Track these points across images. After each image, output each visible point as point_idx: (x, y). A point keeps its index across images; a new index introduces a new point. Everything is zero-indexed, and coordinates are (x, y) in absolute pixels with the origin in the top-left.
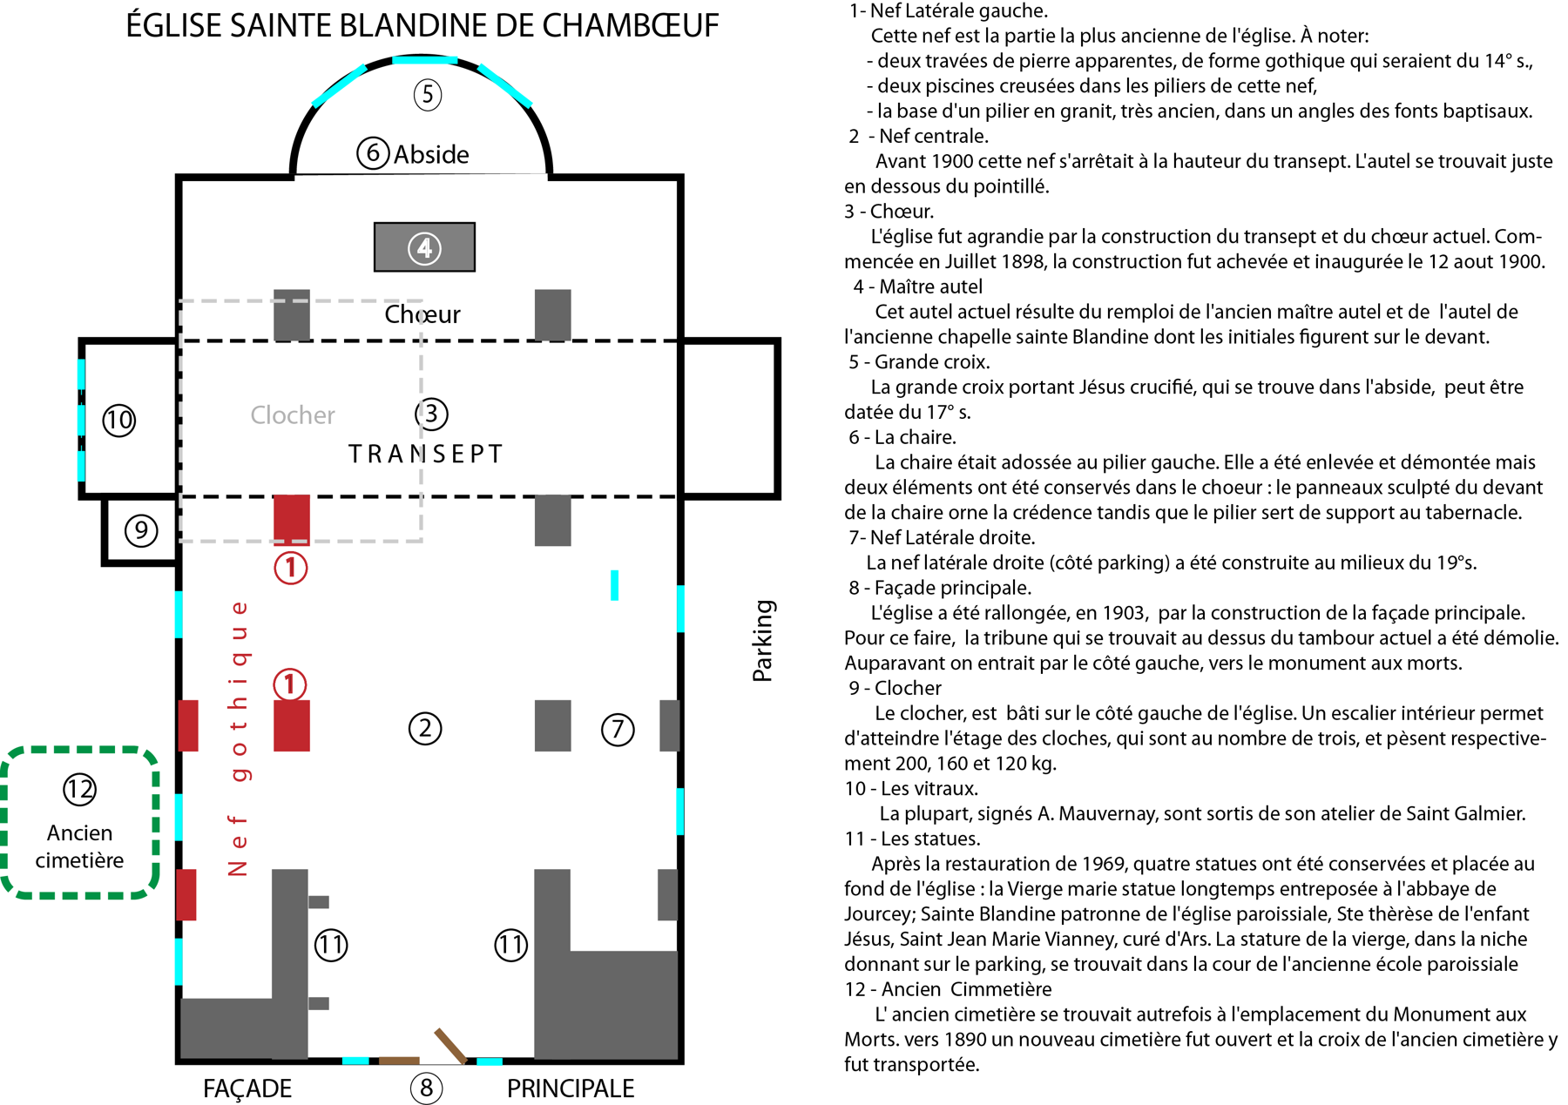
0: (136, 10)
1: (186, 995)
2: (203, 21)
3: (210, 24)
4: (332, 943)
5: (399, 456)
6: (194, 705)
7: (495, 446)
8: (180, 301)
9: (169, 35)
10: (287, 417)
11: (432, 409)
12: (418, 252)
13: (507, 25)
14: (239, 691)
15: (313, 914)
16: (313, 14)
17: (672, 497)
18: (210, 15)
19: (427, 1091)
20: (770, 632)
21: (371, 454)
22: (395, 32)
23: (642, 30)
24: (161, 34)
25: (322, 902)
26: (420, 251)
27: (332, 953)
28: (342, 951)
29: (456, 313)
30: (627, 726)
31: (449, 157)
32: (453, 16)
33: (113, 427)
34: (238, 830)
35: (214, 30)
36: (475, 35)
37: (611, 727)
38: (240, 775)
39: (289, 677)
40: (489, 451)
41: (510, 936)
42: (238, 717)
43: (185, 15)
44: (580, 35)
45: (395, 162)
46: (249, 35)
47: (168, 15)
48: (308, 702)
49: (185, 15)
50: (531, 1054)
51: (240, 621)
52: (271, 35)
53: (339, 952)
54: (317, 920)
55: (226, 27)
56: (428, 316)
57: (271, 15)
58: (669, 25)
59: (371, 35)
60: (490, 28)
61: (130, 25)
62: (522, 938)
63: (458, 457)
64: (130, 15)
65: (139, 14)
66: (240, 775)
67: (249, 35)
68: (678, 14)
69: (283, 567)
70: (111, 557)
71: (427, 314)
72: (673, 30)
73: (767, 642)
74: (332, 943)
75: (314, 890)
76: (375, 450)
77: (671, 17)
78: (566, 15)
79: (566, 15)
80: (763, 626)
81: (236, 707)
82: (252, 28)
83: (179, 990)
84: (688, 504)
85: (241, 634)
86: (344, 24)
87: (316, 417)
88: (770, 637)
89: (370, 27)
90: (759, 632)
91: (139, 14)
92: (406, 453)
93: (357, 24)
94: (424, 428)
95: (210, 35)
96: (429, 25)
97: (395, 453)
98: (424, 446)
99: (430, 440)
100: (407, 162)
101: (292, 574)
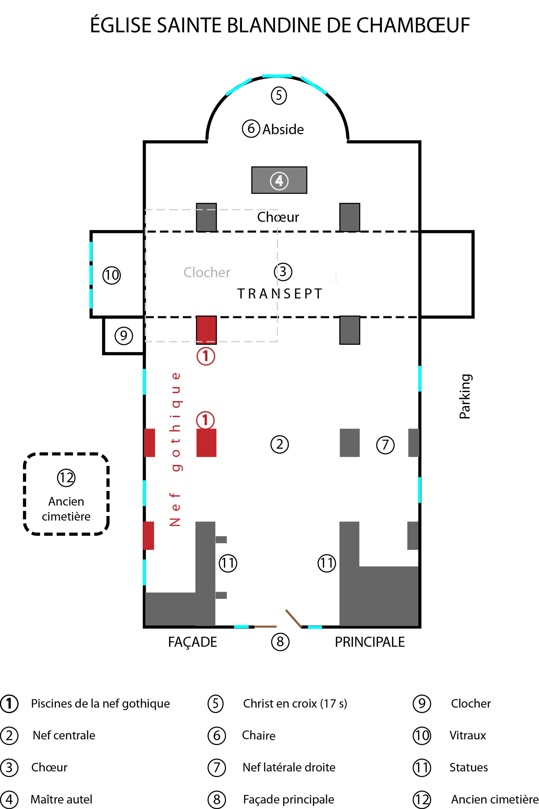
0: (97, 15)
1: (148, 591)
2: (140, 22)
3: (144, 25)
4: (228, 562)
5: (265, 295)
6: (153, 431)
7: (318, 289)
8: (145, 210)
9: (118, 31)
10: (204, 274)
11: (283, 269)
12: (276, 183)
13: (334, 25)
14: (176, 421)
15: (218, 546)
16: (210, 18)
17: (416, 317)
18: (144, 19)
19: (280, 643)
20: (469, 391)
21: (250, 294)
22: (262, 29)
23: (420, 28)
24: (112, 31)
25: (223, 540)
26: (277, 182)
27: (228, 568)
28: (234, 566)
29: (296, 216)
30: (390, 443)
31: (293, 131)
32: (300, 19)
33: (108, 279)
34: (175, 500)
35: (147, 28)
36: (314, 31)
37: (382, 444)
38: (176, 468)
39: (205, 416)
40: (315, 292)
41: (326, 558)
42: (175, 436)
43: (128, 19)
44: (381, 31)
45: (263, 133)
46: (169, 31)
47: (117, 19)
48: (215, 430)
49: (128, 19)
50: (338, 624)
51: (176, 383)
52: (183, 31)
53: (232, 567)
54: (220, 549)
55: (154, 26)
56: (281, 218)
57: (183, 19)
58: (438, 25)
59: (247, 31)
60: (323, 27)
61: (93, 25)
62: (333, 559)
63: (298, 296)
64: (92, 19)
65: (98, 18)
66: (176, 468)
67: (169, 31)
68: (444, 18)
69: (202, 356)
70: (106, 351)
71: (280, 217)
72: (441, 28)
73: (467, 397)
74: (228, 562)
75: (218, 533)
76: (252, 291)
77: (440, 20)
78: (372, 19)
79: (372, 19)
80: (465, 389)
81: (174, 431)
82: (171, 27)
83: (144, 587)
84: (423, 320)
85: (177, 390)
86: (230, 24)
87: (219, 273)
88: (469, 394)
89: (247, 26)
90: (463, 391)
91: (98, 18)
92: (269, 293)
93: (238, 24)
94: (279, 279)
95: (144, 31)
96: (284, 25)
97: (263, 293)
98: (279, 289)
99: (282, 286)
100: (270, 133)
101: (206, 360)
